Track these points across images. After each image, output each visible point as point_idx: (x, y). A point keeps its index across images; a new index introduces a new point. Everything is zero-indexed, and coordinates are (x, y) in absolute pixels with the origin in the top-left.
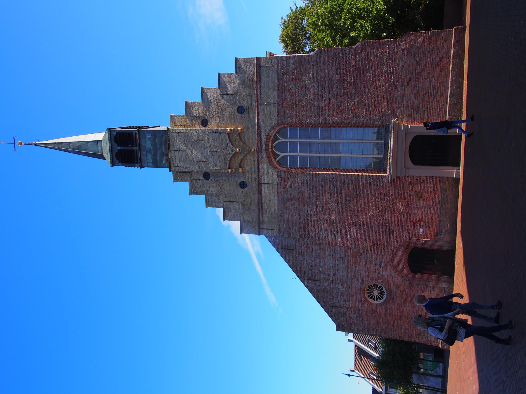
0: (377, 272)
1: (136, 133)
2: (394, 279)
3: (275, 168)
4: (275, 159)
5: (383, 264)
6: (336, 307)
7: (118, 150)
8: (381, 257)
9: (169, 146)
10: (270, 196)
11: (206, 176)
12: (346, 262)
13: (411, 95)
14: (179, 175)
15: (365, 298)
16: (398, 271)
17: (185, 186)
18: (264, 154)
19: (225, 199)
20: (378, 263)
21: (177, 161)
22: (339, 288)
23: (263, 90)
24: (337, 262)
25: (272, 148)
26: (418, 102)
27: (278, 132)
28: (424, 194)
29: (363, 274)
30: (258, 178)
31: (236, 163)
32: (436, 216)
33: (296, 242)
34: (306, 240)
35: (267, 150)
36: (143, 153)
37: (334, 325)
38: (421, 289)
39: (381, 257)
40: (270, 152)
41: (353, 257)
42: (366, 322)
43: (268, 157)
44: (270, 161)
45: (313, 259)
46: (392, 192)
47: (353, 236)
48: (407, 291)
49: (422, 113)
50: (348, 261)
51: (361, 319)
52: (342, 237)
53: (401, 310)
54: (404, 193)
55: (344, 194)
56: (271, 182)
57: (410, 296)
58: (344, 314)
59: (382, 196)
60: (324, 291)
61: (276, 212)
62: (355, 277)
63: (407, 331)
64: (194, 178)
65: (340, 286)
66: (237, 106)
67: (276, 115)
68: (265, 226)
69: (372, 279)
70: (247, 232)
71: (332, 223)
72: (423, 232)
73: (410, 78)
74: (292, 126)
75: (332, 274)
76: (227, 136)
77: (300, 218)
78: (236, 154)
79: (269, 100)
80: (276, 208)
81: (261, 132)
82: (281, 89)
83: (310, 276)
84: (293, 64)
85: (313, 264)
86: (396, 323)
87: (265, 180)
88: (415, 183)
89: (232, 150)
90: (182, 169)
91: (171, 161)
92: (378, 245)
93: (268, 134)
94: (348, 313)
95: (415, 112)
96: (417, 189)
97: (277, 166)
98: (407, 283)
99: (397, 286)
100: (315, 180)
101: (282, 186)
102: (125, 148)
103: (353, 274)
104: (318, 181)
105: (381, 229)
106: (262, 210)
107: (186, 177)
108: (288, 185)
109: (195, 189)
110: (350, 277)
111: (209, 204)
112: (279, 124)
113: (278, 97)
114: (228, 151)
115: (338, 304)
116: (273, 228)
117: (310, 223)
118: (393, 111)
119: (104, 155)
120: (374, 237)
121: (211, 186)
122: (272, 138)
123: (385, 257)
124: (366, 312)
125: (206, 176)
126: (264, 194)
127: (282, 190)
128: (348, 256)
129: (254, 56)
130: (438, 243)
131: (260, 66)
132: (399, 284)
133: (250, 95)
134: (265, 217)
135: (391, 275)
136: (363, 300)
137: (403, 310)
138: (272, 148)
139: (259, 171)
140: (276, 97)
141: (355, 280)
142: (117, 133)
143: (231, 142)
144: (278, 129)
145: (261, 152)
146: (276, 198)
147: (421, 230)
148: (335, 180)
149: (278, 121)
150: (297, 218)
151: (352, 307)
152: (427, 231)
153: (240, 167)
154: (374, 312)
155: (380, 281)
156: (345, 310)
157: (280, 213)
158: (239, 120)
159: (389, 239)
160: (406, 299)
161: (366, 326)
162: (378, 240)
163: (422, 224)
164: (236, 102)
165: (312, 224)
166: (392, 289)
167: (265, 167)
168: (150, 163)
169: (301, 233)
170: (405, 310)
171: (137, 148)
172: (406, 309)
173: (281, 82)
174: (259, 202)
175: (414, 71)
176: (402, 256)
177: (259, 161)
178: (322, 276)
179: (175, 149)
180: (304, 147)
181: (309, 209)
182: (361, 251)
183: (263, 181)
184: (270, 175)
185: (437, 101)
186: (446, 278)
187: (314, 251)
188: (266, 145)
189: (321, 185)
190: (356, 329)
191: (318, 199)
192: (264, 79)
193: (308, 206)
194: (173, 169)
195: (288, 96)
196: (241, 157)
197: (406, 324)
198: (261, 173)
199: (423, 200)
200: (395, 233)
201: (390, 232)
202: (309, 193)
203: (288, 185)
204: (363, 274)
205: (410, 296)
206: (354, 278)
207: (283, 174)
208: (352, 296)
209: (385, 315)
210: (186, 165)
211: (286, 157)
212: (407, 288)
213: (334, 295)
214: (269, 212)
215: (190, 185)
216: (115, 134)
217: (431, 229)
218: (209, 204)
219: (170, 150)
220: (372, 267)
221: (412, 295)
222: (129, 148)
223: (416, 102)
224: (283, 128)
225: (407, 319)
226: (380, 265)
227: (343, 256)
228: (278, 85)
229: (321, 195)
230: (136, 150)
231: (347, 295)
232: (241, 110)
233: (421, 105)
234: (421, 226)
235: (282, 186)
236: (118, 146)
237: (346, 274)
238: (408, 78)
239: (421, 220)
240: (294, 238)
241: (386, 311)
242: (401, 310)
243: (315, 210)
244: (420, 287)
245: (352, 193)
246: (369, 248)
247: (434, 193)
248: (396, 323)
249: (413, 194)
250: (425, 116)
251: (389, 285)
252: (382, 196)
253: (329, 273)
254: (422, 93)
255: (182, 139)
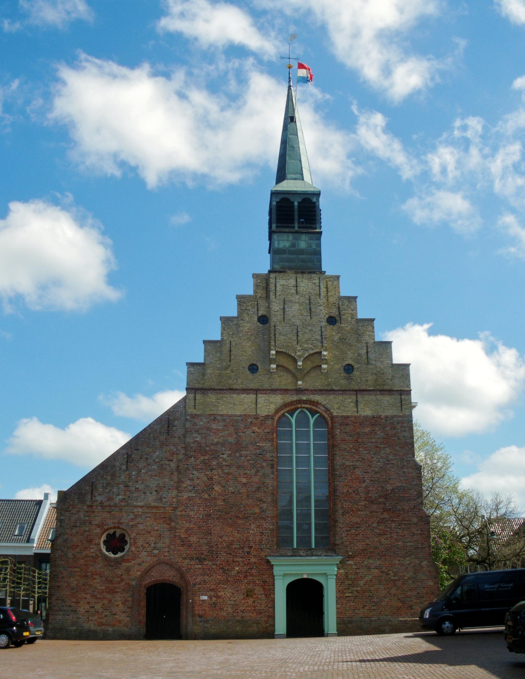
0: (145, 545)
1: (316, 228)
2: (136, 566)
3: (277, 411)
4: (287, 412)
5: (156, 552)
6: (92, 491)
7: (293, 203)
8: (167, 550)
9: (303, 273)
10: (239, 405)
11: (264, 320)
12: (157, 504)
13: (370, 577)
14: (263, 283)
15: (107, 529)
16: (147, 571)
17: (215, 334)
18: (295, 398)
19: (233, 344)
20: (158, 545)
21: (282, 282)
22: (118, 495)
23: (373, 397)
24: (154, 493)
25: (301, 407)
26: (362, 584)
27: (321, 416)
28: (252, 600)
29: (141, 527)
30: (264, 390)
31: (284, 361)
32: (225, 614)
33: (179, 438)
34: (183, 451)
35: (300, 401)
36: (291, 237)
37: (65, 489)
38: (127, 601)
39: (167, 550)
40: (296, 406)
41: (163, 513)
42: (74, 531)
43: (292, 403)
44: (285, 405)
45: (157, 460)
46: (253, 560)
47: (192, 513)
48: (123, 584)
49: (350, 591)
50: (157, 507)
51: (78, 524)
52: (189, 499)
53: (94, 576)
54: (252, 575)
55: (247, 502)
56: (259, 406)
57: (115, 588)
58: (83, 502)
59: (247, 549)
60: (113, 475)
61: (221, 413)
62: (136, 516)
63: (66, 584)
64: (260, 302)
65: (123, 497)
66: (353, 364)
67: (344, 414)
68: (198, 396)
69: (135, 539)
70: (189, 373)
71: (210, 488)
72: (203, 600)
73: (390, 574)
74: (331, 435)
75: (137, 486)
76: (318, 350)
77: (213, 444)
78: (295, 361)
79: (362, 405)
80: (224, 412)
81: (323, 394)
82: (374, 421)
83: (133, 456)
84: (404, 436)
85: (151, 461)
86: (76, 570)
87: (262, 398)
88: (266, 587)
89: (300, 357)
90: (272, 287)
91: (282, 274)
92: (183, 545)
93: (320, 404)
94: (85, 507)
95: (350, 582)
96: (258, 590)
97: (279, 414)
98: (134, 583)
99: (128, 570)
100: (265, 464)
101: (254, 421)
102: (296, 213)
103: (140, 513)
104: (262, 467)
105: (204, 548)
106: (221, 393)
107: (261, 293)
108: (256, 429)
109: (245, 302)
110: (135, 510)
111: (226, 321)
112: (332, 418)
113: (366, 417)
114: (299, 351)
115: (96, 494)
116: (197, 407)
117: (207, 458)
118: (350, 557)
119: (285, 181)
120: (193, 539)
121: (251, 324)
122: (315, 408)
123: (166, 554)
124: (89, 531)
125: (264, 320)
126: (243, 396)
127: (250, 420)
128: (164, 508)
129: (411, 388)
130: (190, 619)
131: (401, 395)
132: (130, 573)
133: (367, 381)
134: (212, 398)
135: (143, 562)
136: (106, 527)
137: (96, 579)
138: (301, 407)
139: (274, 391)
140: (366, 414)
141: (132, 517)
142: (315, 203)
143: (310, 355)
144: (326, 416)
145: (297, 394)
146: (238, 413)
147: (205, 598)
148: (266, 489)
149: (337, 417)
150: (213, 440)
151: (93, 512)
152: (204, 605)
153: (277, 366)
154: (90, 541)
155: (133, 549)
156: (88, 503)
157: (219, 417)
158: (336, 367)
159: (192, 559)
160: (110, 582)
161: (68, 531)
162: (190, 546)
163: (214, 599)
164: (358, 363)
165: (205, 460)
166: (123, 564)
167: (278, 400)
168: (279, 244)
169: (192, 445)
170: (96, 581)
171: (296, 229)
172: (98, 583)
173: (383, 421)
174: (232, 390)
175: (397, 578)
176: (169, 575)
177: (285, 391)
178: (134, 473)
179: (299, 280)
180: (303, 448)
181: (225, 456)
182: (172, 524)
183: (260, 396)
184: (268, 405)
185: (364, 607)
186: (143, 630)
187: (167, 462)
188: (306, 400)
189: (258, 471)
190: (62, 518)
191: (238, 467)
192: (386, 399)
193: (229, 455)
194: (272, 275)
195: (367, 430)
196: (291, 368)
197: (76, 582)
198: (270, 393)
199: (244, 599)
200: (200, 566)
201: (200, 560)
202: (246, 456)
203: (256, 429)
204: (141, 527)
205: (115, 588)
206: (135, 515)
207: (269, 422)
208: (109, 512)
209: (87, 556)
210: (278, 294)
211: (291, 426)
212: (126, 584)
213: (108, 488)
214: (219, 403)
215: (250, 296)
216: (314, 200)
217: (207, 609)
218: (226, 321)
219: (296, 273)
220: (152, 539)
221: (117, 590)
222: (296, 217)
223: (361, 583)
224: (327, 421)
225: (84, 585)
226: (155, 548)
227: (164, 500)
228: (380, 417)
229: (245, 472)
230: (294, 227)
231: (110, 506)
232: (349, 369)
233: (359, 589)
234: (210, 597)
235: (254, 421)
236: (299, 203)
237: (139, 504)
238: (390, 572)
239: (218, 597)
240: (184, 436)
241: (92, 557)
242: (94, 576)
243: (224, 463)
244: (130, 599)
245: (249, 512)
246: (177, 534)
247: (254, 610)
248: (76, 570)
249: (251, 586)
250: (346, 595)
251: (128, 561)
252: (247, 549)
253: (140, 482)
254: (372, 588)
255: (311, 291)
